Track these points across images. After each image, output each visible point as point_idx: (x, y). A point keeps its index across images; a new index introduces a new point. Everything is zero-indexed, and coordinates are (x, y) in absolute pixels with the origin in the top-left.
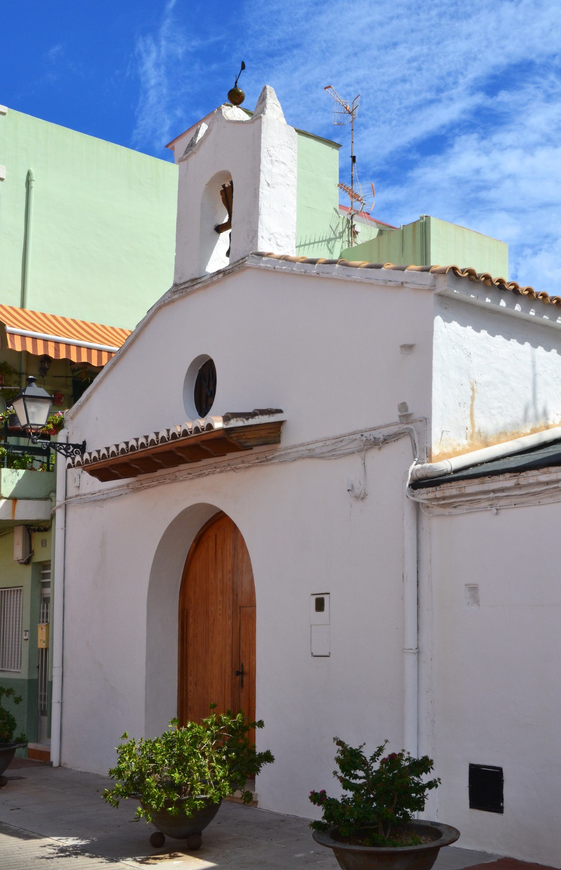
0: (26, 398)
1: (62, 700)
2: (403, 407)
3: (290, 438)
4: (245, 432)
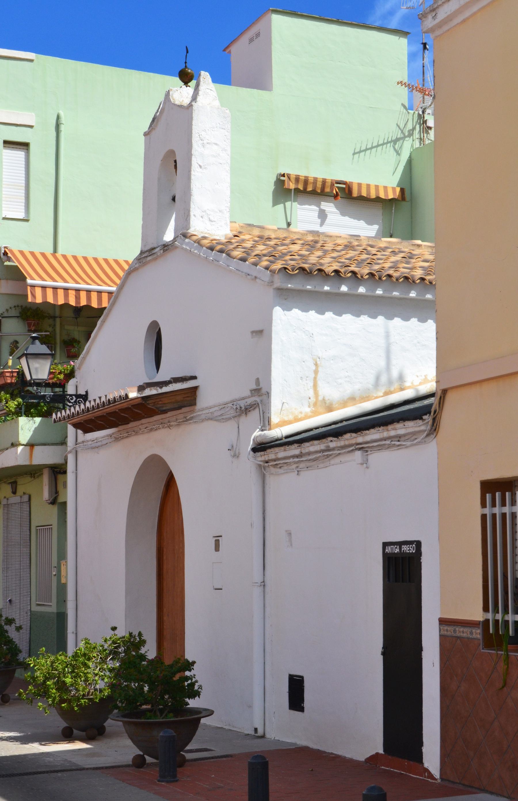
0: (28, 356)
1: (76, 631)
2: (258, 381)
3: (206, 400)
4: (161, 398)
